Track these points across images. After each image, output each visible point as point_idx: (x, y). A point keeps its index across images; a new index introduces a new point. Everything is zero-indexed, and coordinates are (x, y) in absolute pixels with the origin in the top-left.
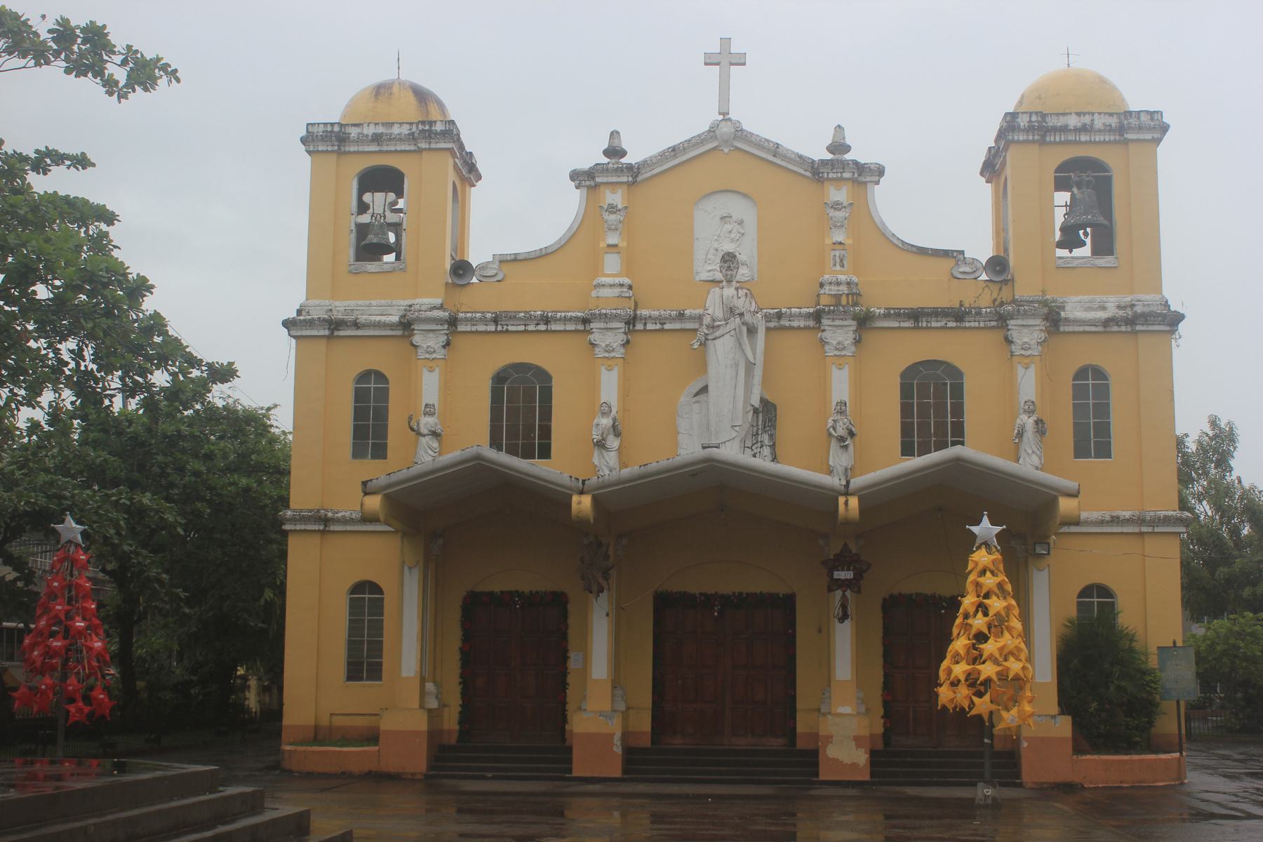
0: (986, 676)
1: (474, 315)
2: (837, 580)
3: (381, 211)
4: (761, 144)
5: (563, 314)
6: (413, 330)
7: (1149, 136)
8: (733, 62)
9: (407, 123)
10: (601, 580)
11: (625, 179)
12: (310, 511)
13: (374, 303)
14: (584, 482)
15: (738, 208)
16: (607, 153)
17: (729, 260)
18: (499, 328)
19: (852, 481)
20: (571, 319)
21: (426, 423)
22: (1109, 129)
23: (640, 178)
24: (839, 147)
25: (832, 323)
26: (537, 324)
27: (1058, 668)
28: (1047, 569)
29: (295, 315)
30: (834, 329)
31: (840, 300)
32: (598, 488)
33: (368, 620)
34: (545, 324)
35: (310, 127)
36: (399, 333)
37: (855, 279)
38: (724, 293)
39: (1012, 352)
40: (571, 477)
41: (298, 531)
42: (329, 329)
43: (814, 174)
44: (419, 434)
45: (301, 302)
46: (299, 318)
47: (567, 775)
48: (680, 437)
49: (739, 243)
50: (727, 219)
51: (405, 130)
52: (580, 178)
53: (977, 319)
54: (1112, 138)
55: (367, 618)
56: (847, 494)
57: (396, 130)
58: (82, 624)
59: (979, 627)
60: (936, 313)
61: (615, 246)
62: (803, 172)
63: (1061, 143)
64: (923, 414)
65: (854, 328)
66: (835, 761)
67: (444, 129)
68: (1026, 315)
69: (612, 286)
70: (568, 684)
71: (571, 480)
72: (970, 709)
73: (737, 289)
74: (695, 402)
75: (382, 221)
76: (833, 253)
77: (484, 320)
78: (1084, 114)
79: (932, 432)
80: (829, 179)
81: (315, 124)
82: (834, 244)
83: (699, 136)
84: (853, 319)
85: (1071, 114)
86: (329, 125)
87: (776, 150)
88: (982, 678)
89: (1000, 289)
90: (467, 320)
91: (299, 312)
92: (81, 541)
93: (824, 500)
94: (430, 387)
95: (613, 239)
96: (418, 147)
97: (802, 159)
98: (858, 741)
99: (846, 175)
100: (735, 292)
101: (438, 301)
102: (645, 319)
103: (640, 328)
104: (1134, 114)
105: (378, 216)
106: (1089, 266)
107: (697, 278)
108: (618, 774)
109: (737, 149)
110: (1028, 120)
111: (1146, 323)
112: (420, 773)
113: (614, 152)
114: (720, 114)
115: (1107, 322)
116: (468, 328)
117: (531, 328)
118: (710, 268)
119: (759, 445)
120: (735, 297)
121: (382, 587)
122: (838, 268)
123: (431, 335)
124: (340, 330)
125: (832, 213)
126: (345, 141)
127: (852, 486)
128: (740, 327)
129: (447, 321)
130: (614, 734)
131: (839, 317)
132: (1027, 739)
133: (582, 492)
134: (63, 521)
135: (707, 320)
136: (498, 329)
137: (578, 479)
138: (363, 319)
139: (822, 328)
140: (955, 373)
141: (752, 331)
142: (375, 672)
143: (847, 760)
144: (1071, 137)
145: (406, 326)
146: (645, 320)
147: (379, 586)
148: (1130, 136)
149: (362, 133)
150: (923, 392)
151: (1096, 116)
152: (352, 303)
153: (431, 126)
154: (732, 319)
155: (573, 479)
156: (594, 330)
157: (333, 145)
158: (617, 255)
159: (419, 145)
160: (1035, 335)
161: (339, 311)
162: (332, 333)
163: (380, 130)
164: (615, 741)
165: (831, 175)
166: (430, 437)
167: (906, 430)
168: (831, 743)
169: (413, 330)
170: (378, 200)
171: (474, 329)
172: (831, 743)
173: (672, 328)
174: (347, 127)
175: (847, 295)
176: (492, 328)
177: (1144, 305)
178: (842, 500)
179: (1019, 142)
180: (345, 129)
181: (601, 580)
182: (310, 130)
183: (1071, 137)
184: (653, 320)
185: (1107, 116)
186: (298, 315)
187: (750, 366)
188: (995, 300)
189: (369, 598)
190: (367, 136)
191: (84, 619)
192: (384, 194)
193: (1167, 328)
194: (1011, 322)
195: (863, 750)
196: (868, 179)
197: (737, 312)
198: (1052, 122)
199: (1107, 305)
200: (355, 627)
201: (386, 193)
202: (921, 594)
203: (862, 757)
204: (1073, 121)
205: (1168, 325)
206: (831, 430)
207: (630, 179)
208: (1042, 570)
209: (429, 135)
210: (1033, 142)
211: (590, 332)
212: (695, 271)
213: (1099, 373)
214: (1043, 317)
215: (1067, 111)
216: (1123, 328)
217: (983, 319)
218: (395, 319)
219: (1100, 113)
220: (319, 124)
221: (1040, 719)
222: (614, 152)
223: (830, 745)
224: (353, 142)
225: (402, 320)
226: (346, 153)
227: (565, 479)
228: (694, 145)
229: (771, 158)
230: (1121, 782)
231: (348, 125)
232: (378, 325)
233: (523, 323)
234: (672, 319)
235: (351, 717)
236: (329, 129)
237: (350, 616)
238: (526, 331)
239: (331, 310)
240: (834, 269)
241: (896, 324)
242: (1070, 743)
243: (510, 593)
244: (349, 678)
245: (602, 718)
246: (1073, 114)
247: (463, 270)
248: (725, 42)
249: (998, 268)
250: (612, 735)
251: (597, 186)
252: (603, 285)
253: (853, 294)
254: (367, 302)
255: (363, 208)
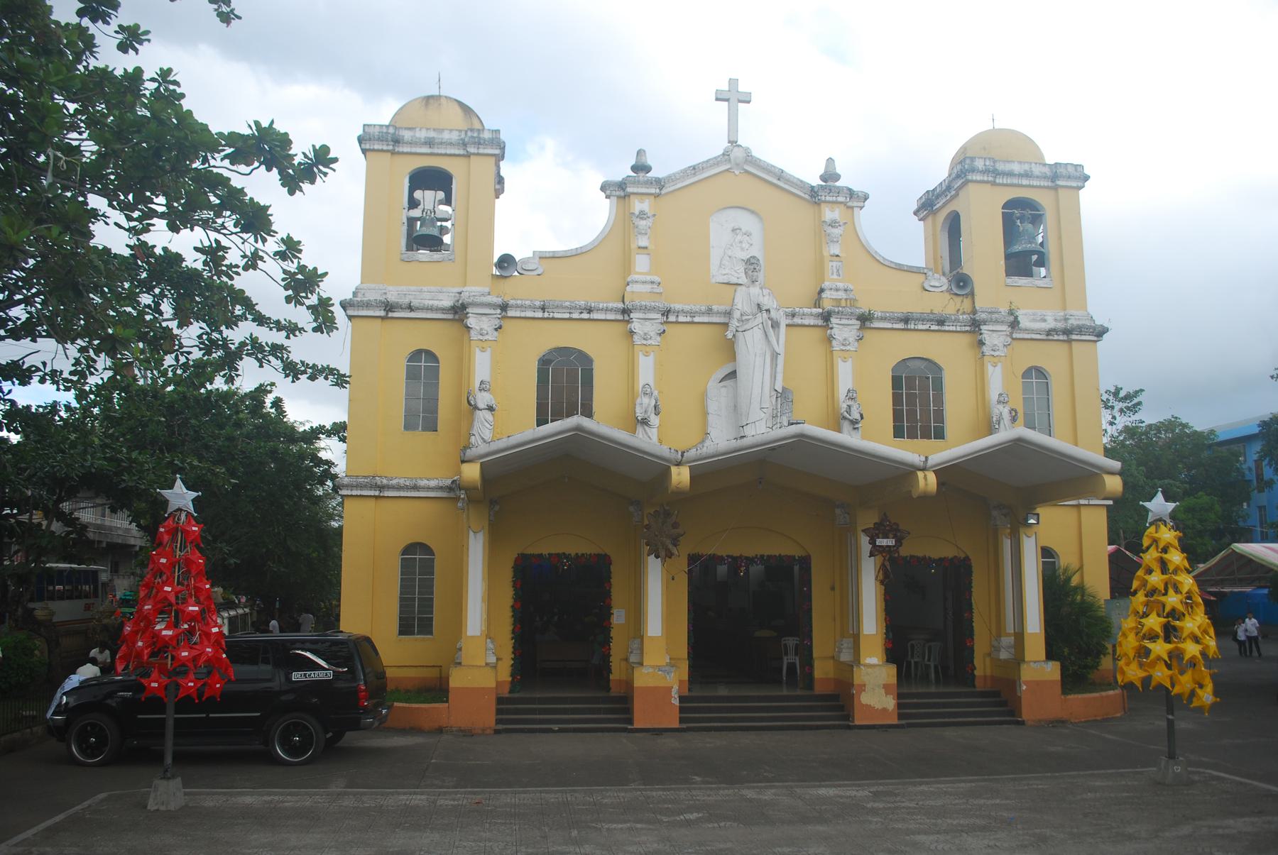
0: (1198, 653)
1: (524, 302)
2: (880, 546)
3: (431, 208)
4: (768, 169)
5: (605, 305)
6: (468, 313)
7: (1074, 184)
8: (740, 99)
9: (457, 130)
10: (671, 547)
11: (653, 191)
12: (365, 477)
13: (425, 289)
14: (683, 453)
15: (746, 221)
16: (635, 169)
17: (751, 264)
18: (546, 315)
19: (930, 458)
20: (611, 310)
21: (483, 399)
22: (1045, 177)
23: (663, 192)
24: (830, 176)
25: (840, 322)
26: (581, 313)
27: (1045, 621)
28: (1034, 537)
29: (351, 296)
30: (841, 327)
31: (840, 302)
32: (694, 461)
33: (419, 579)
34: (588, 313)
35: (366, 127)
36: (450, 316)
37: (851, 287)
38: (751, 292)
39: (983, 352)
40: (670, 449)
41: (354, 496)
42: (384, 310)
43: (812, 196)
44: (476, 408)
45: (357, 285)
46: (356, 299)
47: (629, 727)
48: (710, 418)
49: (748, 251)
50: (738, 231)
51: (454, 136)
52: (611, 189)
53: (955, 324)
54: (1046, 184)
55: (417, 577)
56: (924, 469)
57: (446, 136)
58: (197, 608)
59: (1173, 604)
60: (922, 319)
61: (646, 248)
62: (803, 195)
63: (1007, 185)
64: (911, 400)
65: (858, 327)
66: (868, 706)
67: (491, 137)
68: (997, 322)
69: (644, 282)
70: (612, 638)
71: (670, 452)
72: (1173, 686)
73: (761, 288)
74: (722, 387)
75: (433, 216)
76: (831, 264)
77: (534, 308)
78: (1025, 163)
79: (918, 418)
80: (825, 202)
81: (371, 125)
82: (831, 256)
83: (715, 158)
84: (857, 320)
85: (1014, 162)
86: (384, 127)
87: (780, 175)
88: (1187, 657)
89: (962, 301)
90: (517, 306)
91: (355, 294)
92: (192, 509)
93: (661, 470)
94: (481, 366)
95: (643, 242)
96: (467, 152)
97: (801, 184)
98: (886, 687)
99: (841, 199)
100: (761, 291)
101: (487, 290)
102: (678, 312)
103: (672, 320)
104: (1062, 165)
105: (429, 212)
106: (1030, 285)
107: (713, 281)
108: (675, 724)
109: (747, 172)
110: (983, 164)
111: (1080, 333)
112: (490, 728)
113: (641, 168)
114: (729, 143)
115: (1049, 332)
116: (518, 314)
117: (575, 316)
118: (724, 272)
119: (779, 425)
120: (761, 295)
121: (433, 548)
122: (835, 277)
123: (484, 318)
124: (394, 312)
125: (830, 230)
126: (399, 143)
127: (930, 463)
128: (766, 321)
129: (500, 306)
130: (672, 687)
131: (845, 317)
132: (1026, 683)
133: (679, 464)
134: (171, 487)
135: (737, 314)
136: (545, 316)
137: (677, 451)
138: (415, 303)
139: (831, 326)
140: (935, 368)
141: (775, 325)
142: (426, 627)
143: (878, 706)
144: (1015, 181)
145: (459, 311)
146: (678, 313)
147: (429, 547)
148: (1060, 183)
149: (415, 136)
150: (910, 386)
151: (1033, 165)
152: (404, 288)
153: (479, 134)
154: (760, 314)
155: (672, 451)
156: (634, 320)
157: (388, 145)
158: (647, 256)
159: (468, 150)
160: (1002, 339)
161: (392, 295)
162: (387, 314)
163: (432, 134)
164: (673, 694)
165: (828, 198)
166: (487, 411)
167: (897, 416)
168: (864, 691)
169: (468, 313)
170: (428, 197)
171: (523, 314)
172: (864, 691)
173: (701, 321)
174: (401, 130)
175: (846, 299)
176: (540, 314)
177: (1076, 319)
178: (920, 474)
179: (976, 181)
180: (399, 132)
181: (671, 547)
182: (366, 130)
183: (1015, 181)
184: (684, 313)
185: (1041, 166)
186: (354, 297)
187: (775, 355)
188: (959, 310)
189: (419, 558)
190: (420, 138)
191: (197, 603)
192: (433, 192)
193: (1095, 339)
194: (983, 327)
195: (892, 696)
196: (855, 204)
197: (764, 308)
198: (1001, 167)
199: (1046, 317)
200: (406, 586)
201: (436, 191)
202: (914, 556)
203: (890, 703)
204: (1016, 168)
205: (1095, 336)
206: (845, 414)
207: (658, 191)
208: (1029, 537)
209: (479, 143)
210: (987, 182)
211: (628, 322)
212: (711, 275)
213: (1040, 372)
214: (1009, 324)
215: (1010, 160)
216: (1061, 337)
217: (959, 324)
218: (447, 303)
219: (1036, 164)
220: (375, 125)
221: (1036, 665)
222: (641, 168)
223: (863, 693)
224: (406, 143)
225: (456, 304)
226: (399, 153)
227: (664, 451)
228: (711, 166)
229: (775, 181)
230: (1096, 716)
231: (402, 128)
232: (430, 309)
233: (568, 311)
234: (702, 313)
235: (405, 669)
236: (385, 130)
237: (401, 575)
238: (570, 319)
239: (385, 293)
240: (832, 277)
241: (889, 325)
242: (1060, 684)
243: (558, 555)
244: (401, 633)
245: (660, 672)
246: (1016, 163)
247: (508, 263)
248: (733, 83)
249: (961, 284)
250: (670, 689)
251: (627, 196)
252: (636, 282)
253: (851, 300)
254: (419, 288)
255: (413, 204)
